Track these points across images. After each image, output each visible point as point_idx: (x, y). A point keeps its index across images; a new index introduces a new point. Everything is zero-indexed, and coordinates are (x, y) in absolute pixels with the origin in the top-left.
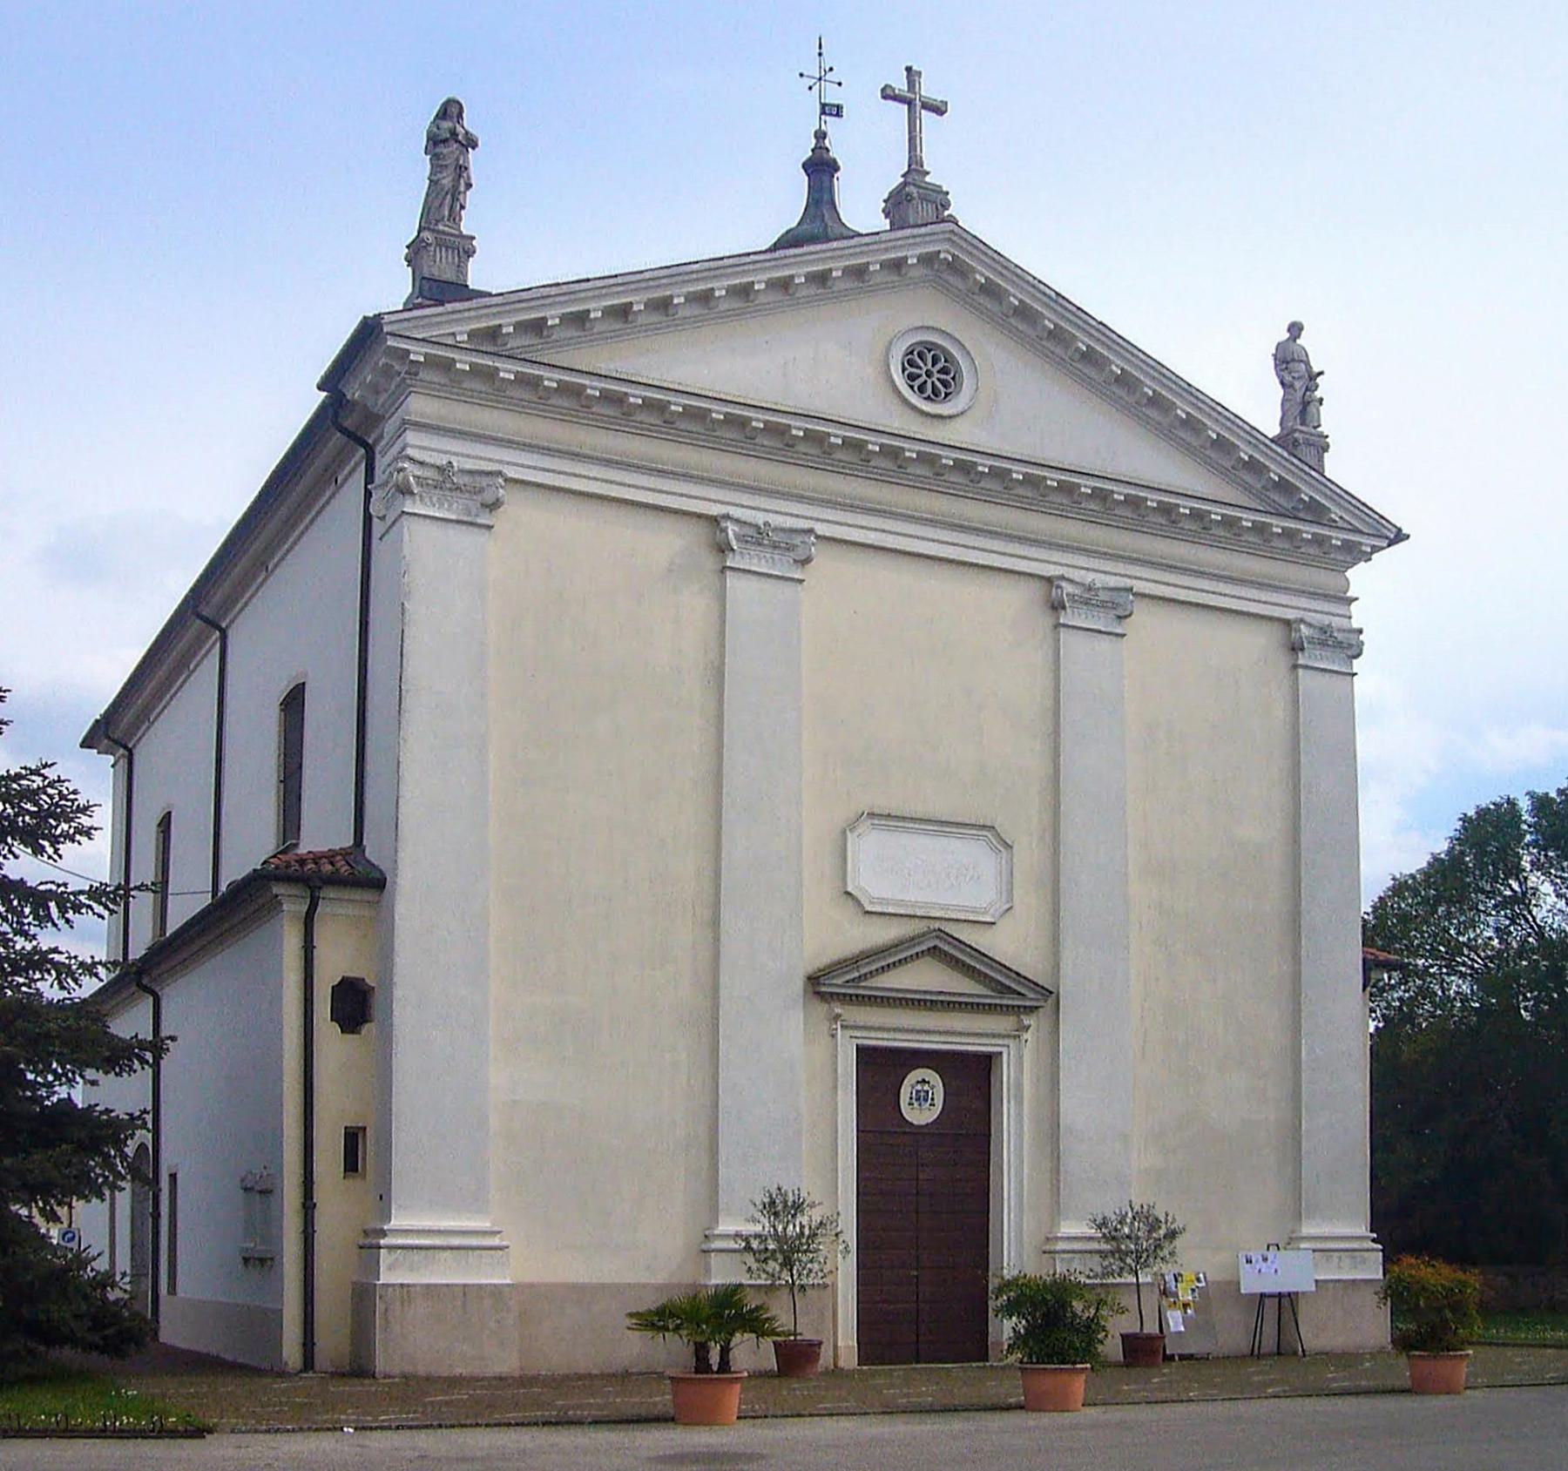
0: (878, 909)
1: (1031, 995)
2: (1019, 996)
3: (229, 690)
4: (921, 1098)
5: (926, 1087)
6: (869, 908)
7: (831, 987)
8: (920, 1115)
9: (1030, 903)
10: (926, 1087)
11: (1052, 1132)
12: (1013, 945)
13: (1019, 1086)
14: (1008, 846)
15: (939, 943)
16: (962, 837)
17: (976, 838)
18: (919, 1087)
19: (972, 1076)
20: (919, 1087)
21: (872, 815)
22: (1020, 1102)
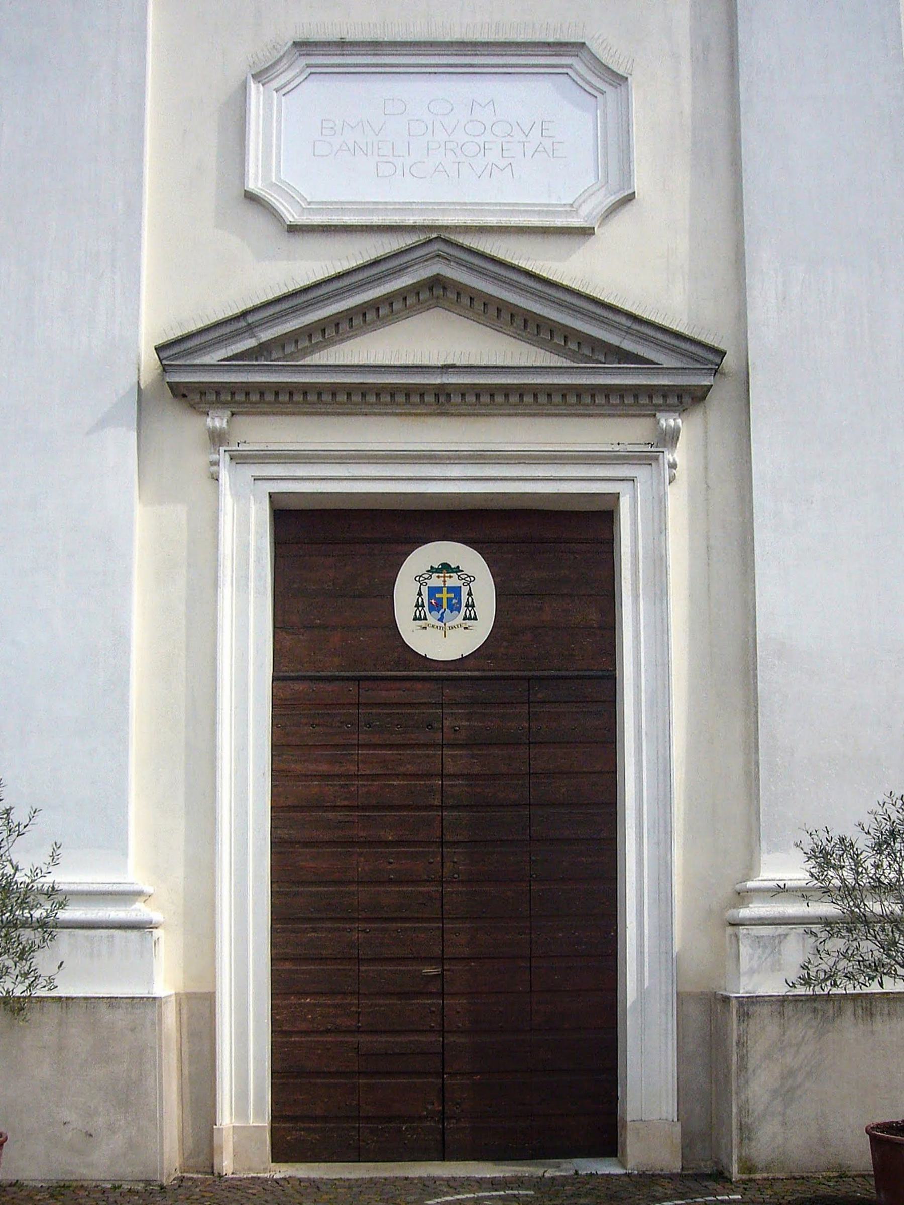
0: (317, 220)
1: (667, 361)
2: (664, 375)
3: (575, 482)
4: (442, 602)
5: (453, 581)
6: (292, 216)
7: (215, 379)
8: (445, 642)
9: (665, 182)
10: (453, 581)
11: (737, 665)
12: (639, 270)
13: (659, 563)
14: (619, 80)
15: (440, 268)
16: (507, 71)
17: (553, 71)
18: (436, 581)
19: (558, 556)
20: (436, 581)
21: (304, 46)
22: (661, 594)
